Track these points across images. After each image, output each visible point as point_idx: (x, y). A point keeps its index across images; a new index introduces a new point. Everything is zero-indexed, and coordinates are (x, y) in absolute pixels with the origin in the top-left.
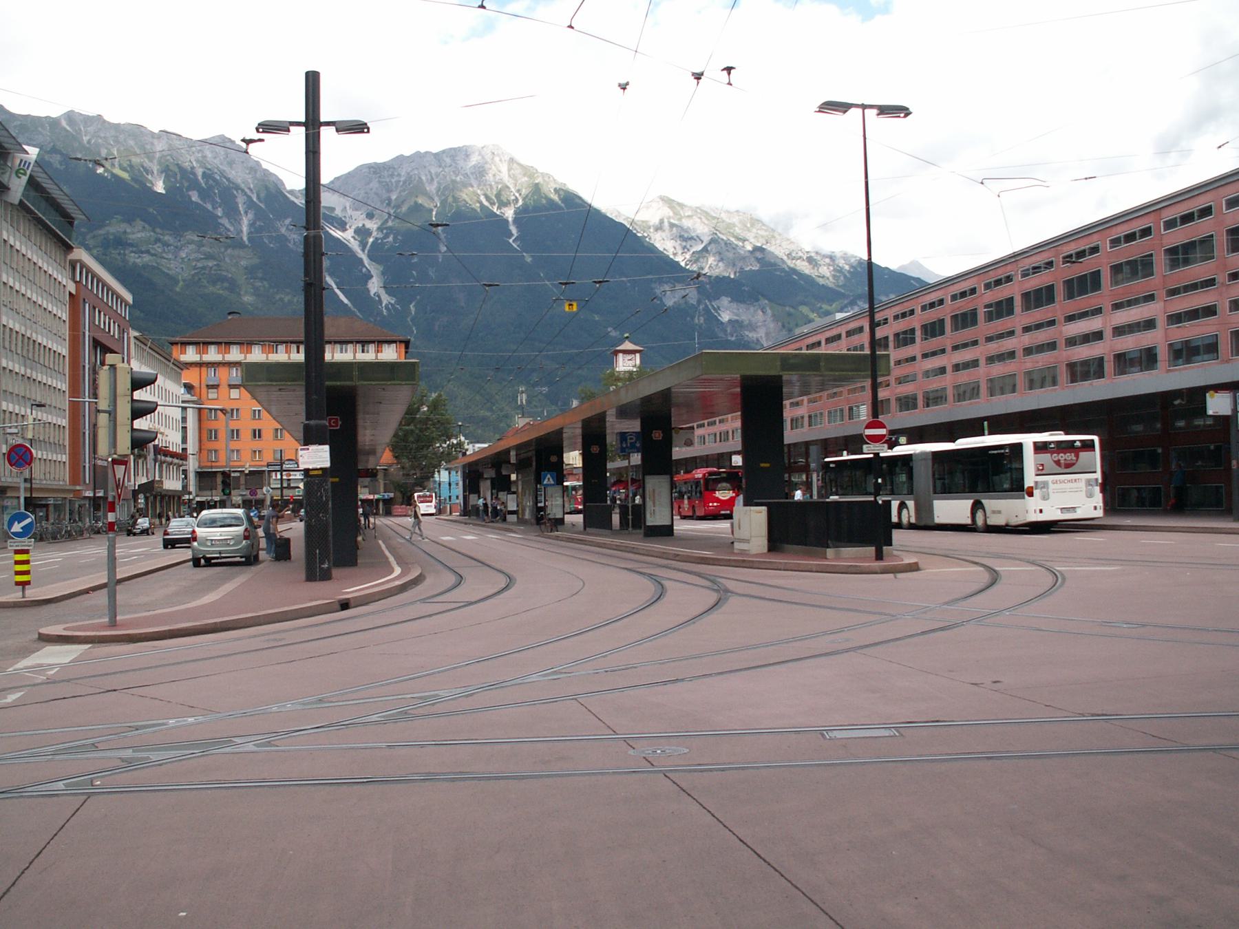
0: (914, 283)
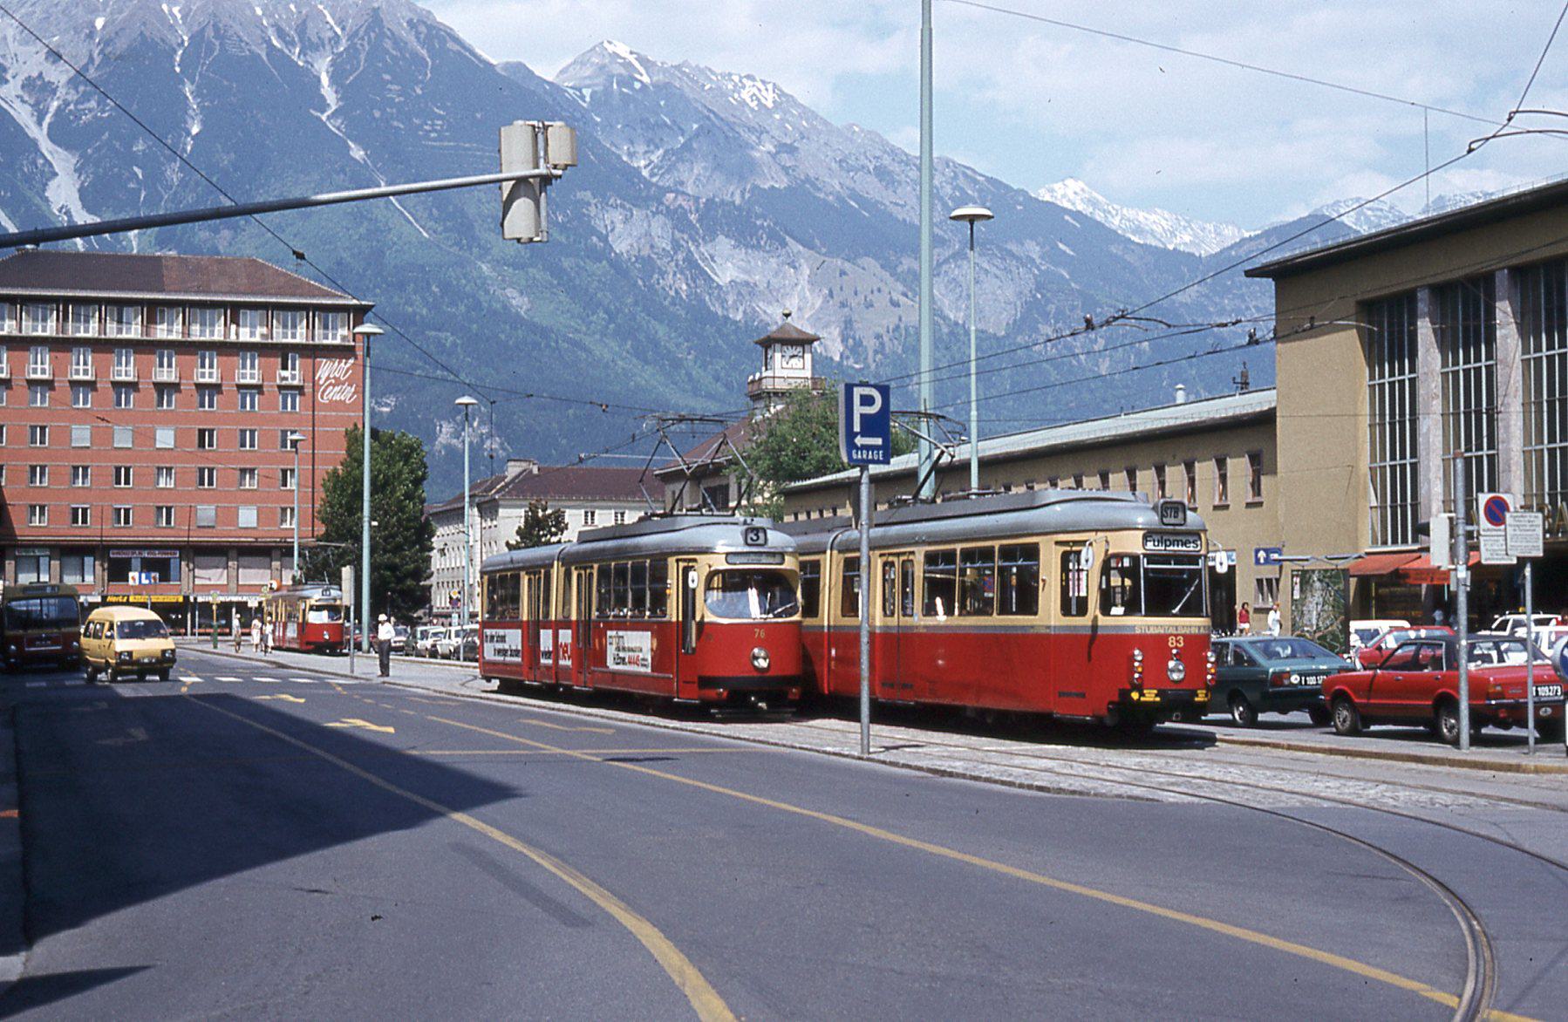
0: (1071, 221)
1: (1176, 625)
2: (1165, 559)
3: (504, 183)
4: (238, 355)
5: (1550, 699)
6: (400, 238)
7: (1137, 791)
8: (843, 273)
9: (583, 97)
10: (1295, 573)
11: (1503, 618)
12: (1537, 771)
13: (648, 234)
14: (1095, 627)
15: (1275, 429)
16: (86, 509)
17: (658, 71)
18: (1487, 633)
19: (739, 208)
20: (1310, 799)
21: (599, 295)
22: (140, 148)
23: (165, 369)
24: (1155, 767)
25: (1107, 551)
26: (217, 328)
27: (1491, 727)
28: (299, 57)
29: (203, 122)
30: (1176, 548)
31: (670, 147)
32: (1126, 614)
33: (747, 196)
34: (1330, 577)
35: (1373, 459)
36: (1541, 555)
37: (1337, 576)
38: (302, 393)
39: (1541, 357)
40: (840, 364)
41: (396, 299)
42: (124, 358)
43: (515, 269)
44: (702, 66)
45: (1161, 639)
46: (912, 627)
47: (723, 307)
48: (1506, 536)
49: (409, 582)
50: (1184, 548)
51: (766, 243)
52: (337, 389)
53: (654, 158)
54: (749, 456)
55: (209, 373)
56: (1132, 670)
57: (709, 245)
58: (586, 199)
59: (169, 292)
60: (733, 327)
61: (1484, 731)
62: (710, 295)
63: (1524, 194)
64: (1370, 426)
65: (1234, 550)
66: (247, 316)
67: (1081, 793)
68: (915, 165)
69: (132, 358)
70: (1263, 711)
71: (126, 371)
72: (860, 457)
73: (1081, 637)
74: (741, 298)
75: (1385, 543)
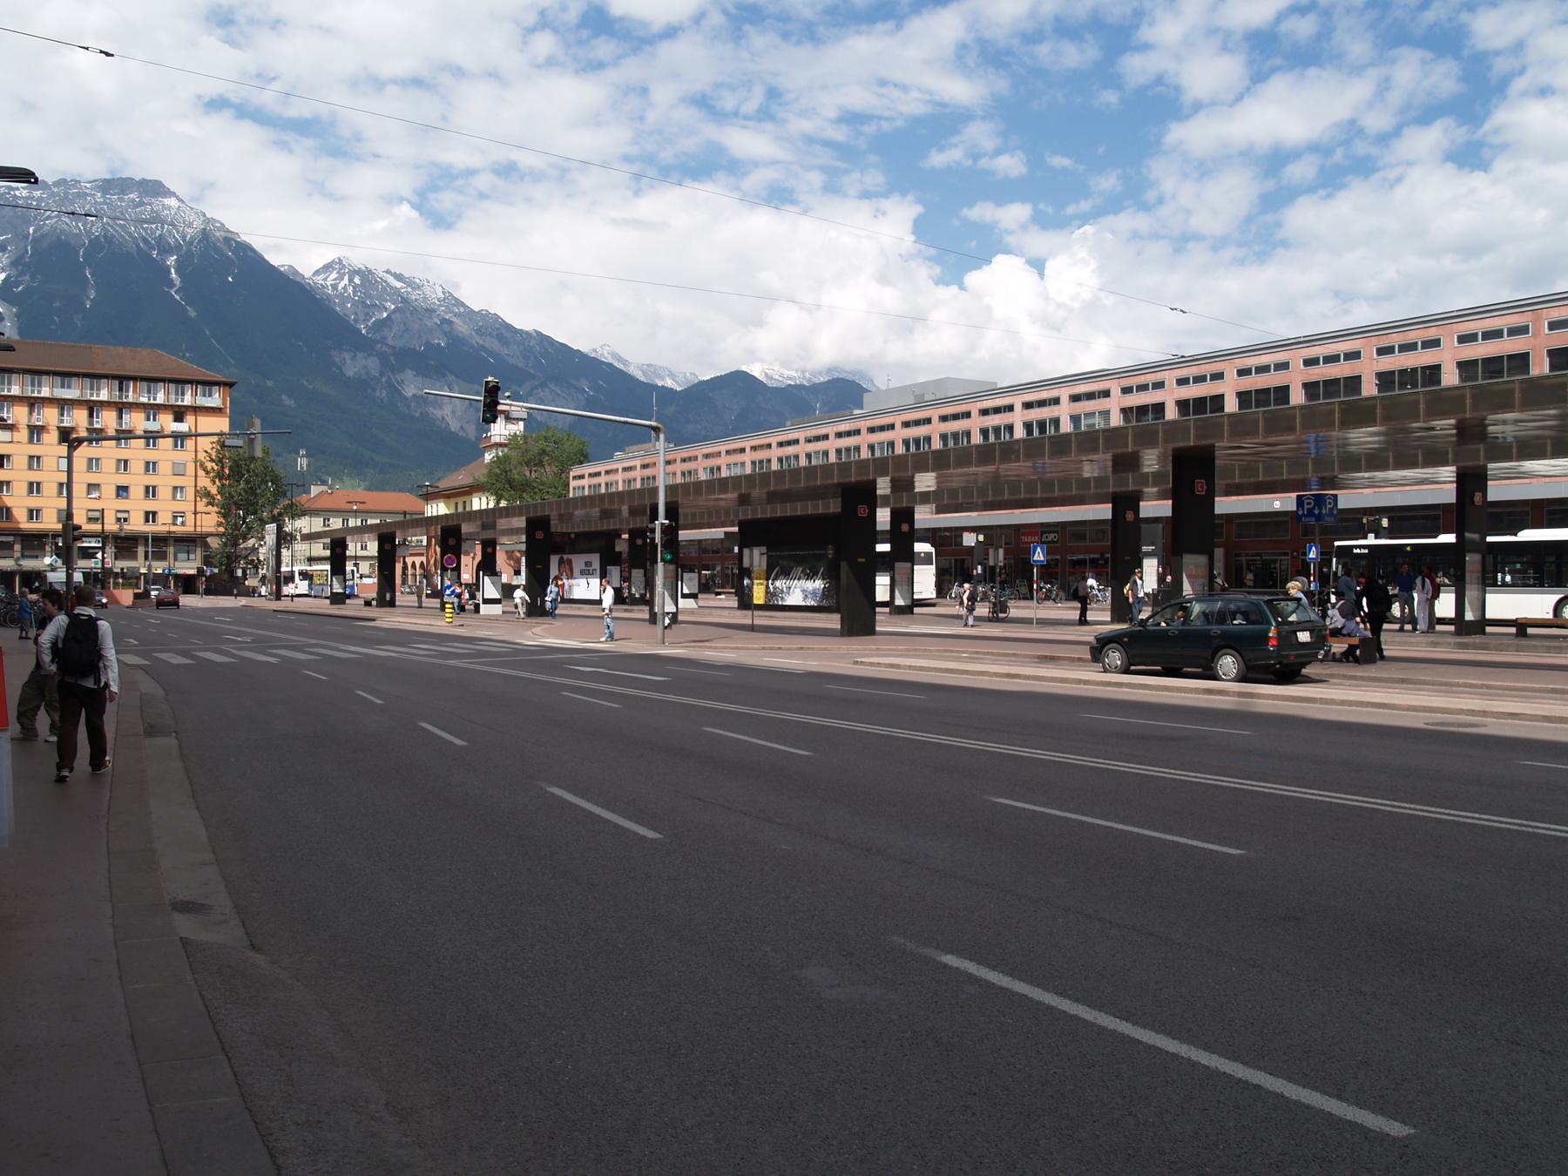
18: (433, 543)
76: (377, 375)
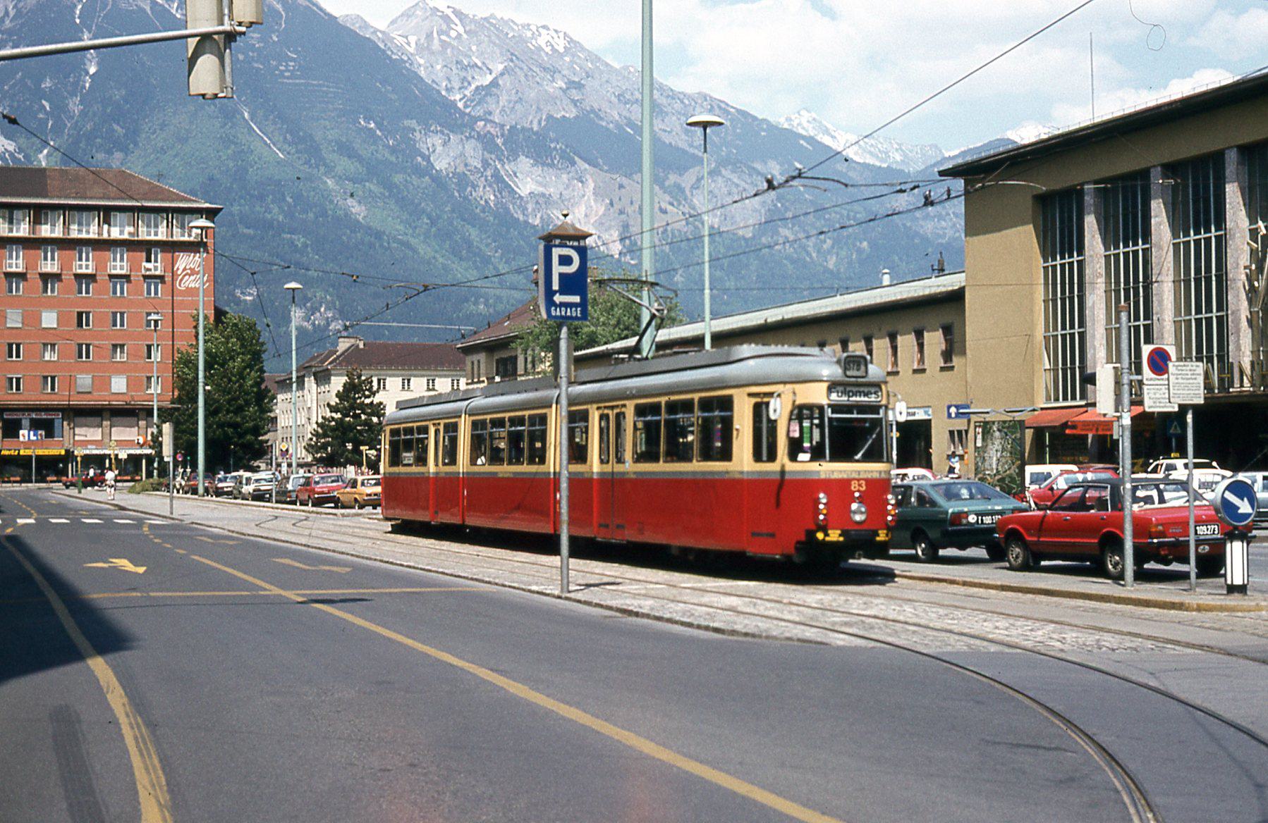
0: (805, 144)
1: (857, 470)
2: (848, 408)
3: (189, 39)
4: (109, 250)
5: (1207, 537)
6: (260, 159)
7: (810, 633)
8: (621, 186)
9: (408, 44)
10: (977, 424)
11: (1158, 462)
12: (1199, 609)
13: (462, 154)
14: (783, 472)
15: (964, 306)
16: (20, 378)
17: (471, 22)
19: (536, 133)
20: (978, 642)
21: (423, 205)
22: (48, 85)
23: (49, 262)
24: (834, 604)
25: (794, 401)
26: (92, 228)
27: (1152, 562)
28: (177, 11)
29: (98, 64)
30: (858, 399)
31: (479, 84)
32: (812, 460)
33: (543, 123)
34: (1008, 428)
35: (1047, 330)
36: (1202, 402)
37: (1014, 427)
38: (163, 282)
39: (1189, 241)
40: (619, 261)
41: (258, 208)
42: (14, 253)
43: (354, 183)
44: (506, 18)
45: (844, 484)
46: (623, 473)
47: (524, 214)
48: (1168, 385)
49: (249, 437)
50: (866, 399)
51: (558, 162)
52: (192, 278)
53: (467, 93)
54: (532, 332)
55: (86, 265)
56: (818, 512)
57: (513, 163)
58: (412, 126)
59: (52, 198)
60: (532, 231)
61: (1146, 566)
62: (513, 204)
63: (1175, 102)
64: (1044, 301)
65: (929, 407)
66: (118, 217)
67: (753, 636)
68: (679, 99)
69: (21, 253)
70: (944, 548)
71: (16, 264)
72: (558, 314)
73: (773, 481)
74: (538, 206)
75: (1057, 400)
76: (479, 166)
